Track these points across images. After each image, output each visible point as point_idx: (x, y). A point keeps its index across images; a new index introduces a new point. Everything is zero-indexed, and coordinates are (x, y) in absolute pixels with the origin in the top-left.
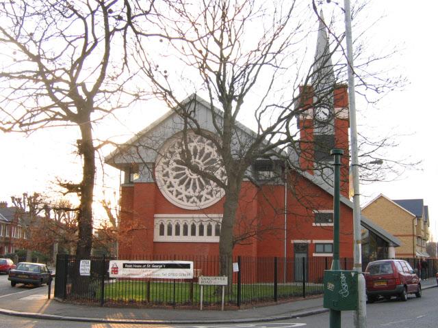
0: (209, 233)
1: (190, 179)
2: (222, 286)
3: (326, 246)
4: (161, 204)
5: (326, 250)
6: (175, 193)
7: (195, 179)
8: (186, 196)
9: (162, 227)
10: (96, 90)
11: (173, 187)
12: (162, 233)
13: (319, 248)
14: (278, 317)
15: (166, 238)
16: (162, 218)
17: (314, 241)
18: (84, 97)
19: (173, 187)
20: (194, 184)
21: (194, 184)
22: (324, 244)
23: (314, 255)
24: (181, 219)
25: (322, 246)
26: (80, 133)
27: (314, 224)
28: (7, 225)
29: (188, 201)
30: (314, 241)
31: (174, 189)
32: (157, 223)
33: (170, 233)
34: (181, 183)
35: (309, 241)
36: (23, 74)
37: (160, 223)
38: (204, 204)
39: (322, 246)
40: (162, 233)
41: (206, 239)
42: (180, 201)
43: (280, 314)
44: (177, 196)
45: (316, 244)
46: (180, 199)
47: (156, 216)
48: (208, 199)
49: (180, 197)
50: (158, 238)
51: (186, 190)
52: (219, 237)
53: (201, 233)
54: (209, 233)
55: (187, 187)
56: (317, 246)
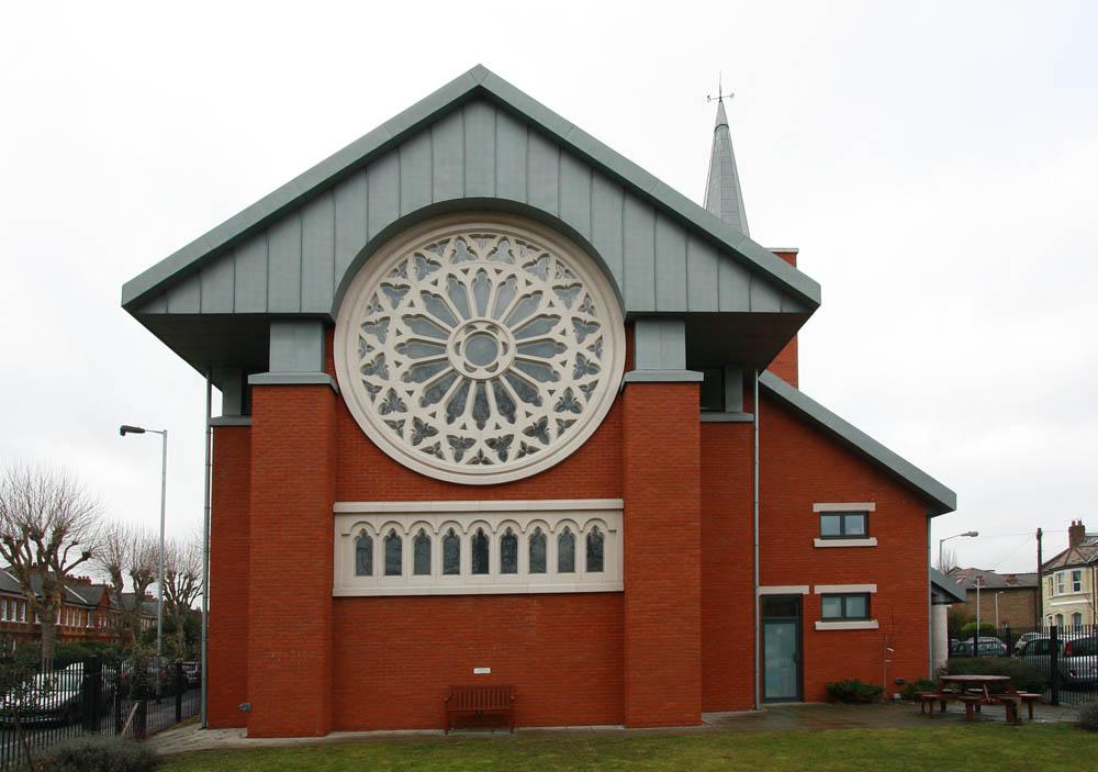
1: (467, 381)
3: (838, 533)
4: (356, 465)
5: (849, 613)
7: (481, 382)
8: (452, 440)
12: (364, 567)
13: (830, 609)
15: (379, 584)
16: (362, 518)
17: (820, 589)
20: (481, 399)
21: (481, 399)
22: (843, 596)
23: (820, 626)
24: (436, 518)
26: (331, 307)
28: (88, 610)
29: (416, 442)
30: (820, 589)
34: (433, 395)
35: (804, 590)
37: (356, 532)
38: (515, 468)
40: (364, 567)
42: (432, 459)
44: (385, 410)
45: (867, 536)
46: (428, 451)
47: (340, 507)
48: (532, 450)
49: (395, 416)
50: (349, 583)
51: (424, 404)
56: (862, 613)
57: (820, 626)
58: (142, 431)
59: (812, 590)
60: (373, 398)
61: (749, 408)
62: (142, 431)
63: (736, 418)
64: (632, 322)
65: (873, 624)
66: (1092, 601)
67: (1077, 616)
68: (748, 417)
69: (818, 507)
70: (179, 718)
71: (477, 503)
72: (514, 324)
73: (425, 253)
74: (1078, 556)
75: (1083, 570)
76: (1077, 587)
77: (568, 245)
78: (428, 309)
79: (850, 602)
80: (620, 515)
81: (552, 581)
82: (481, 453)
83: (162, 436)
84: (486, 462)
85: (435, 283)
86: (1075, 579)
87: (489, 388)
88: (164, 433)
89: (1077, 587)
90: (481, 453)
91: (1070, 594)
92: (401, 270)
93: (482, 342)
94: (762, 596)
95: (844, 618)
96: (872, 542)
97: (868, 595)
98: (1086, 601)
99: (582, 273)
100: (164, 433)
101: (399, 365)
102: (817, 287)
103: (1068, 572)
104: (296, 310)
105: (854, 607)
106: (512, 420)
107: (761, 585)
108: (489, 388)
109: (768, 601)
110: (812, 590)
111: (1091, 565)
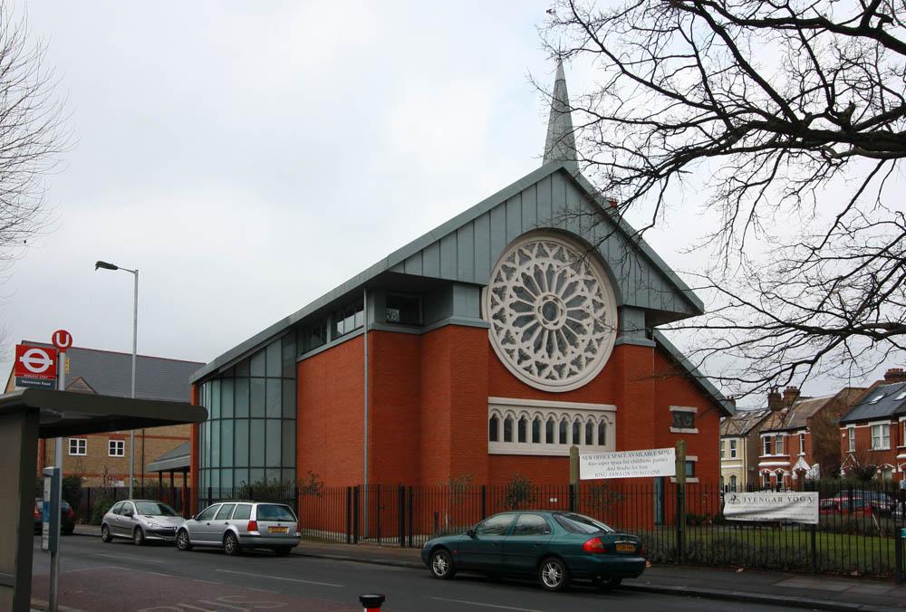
16: (502, 406)
47: (492, 400)
64: (621, 309)
66: (743, 466)
67: (733, 478)
71: (550, 402)
72: (572, 306)
73: (524, 250)
74: (734, 428)
75: (737, 439)
76: (733, 454)
77: (599, 266)
80: (614, 414)
83: (134, 275)
84: (531, 372)
86: (732, 447)
87: (539, 329)
88: (136, 272)
89: (733, 454)
91: (782, 455)
92: (512, 259)
93: (550, 310)
98: (739, 466)
99: (597, 274)
100: (136, 272)
101: (573, 352)
102: (702, 304)
104: (472, 282)
106: (535, 351)
108: (539, 329)
109: (76, 441)
111: (742, 436)
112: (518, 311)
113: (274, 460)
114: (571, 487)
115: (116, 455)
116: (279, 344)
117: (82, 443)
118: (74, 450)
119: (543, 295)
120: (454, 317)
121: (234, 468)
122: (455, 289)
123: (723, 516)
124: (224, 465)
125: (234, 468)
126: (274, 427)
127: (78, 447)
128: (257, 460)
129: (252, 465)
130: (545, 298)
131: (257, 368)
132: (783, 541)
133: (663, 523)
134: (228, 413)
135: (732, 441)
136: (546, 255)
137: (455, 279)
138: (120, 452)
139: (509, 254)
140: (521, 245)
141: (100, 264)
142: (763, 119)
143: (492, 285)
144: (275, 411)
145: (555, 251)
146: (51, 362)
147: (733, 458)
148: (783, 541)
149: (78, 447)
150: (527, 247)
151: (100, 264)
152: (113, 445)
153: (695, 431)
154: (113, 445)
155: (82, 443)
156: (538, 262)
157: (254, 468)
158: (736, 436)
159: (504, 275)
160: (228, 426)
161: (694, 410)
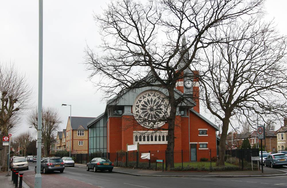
0: (163, 140)
2: (257, 161)
5: (204, 147)
6: (138, 104)
9: (136, 137)
10: (196, 69)
11: (140, 102)
13: (201, 146)
14: (153, 175)
17: (199, 143)
18: (193, 75)
19: (140, 102)
21: (154, 103)
22: (203, 144)
23: (199, 149)
25: (202, 145)
27: (199, 135)
30: (199, 143)
31: (139, 104)
32: (135, 135)
33: (144, 140)
35: (197, 143)
36: (204, 82)
39: (202, 145)
41: (162, 142)
43: (153, 175)
47: (166, 142)
52: (167, 143)
53: (160, 140)
54: (163, 140)
55: (148, 101)
56: (206, 147)
57: (199, 149)
58: (66, 105)
59: (198, 143)
60: (136, 110)
61: (188, 115)
62: (66, 105)
63: (186, 117)
65: (208, 149)
67: (283, 146)
68: (188, 117)
69: (199, 129)
70: (173, 143)
76: (283, 139)
78: (167, 136)
79: (204, 145)
81: (158, 142)
82: (138, 103)
83: (70, 106)
85: (149, 98)
89: (283, 139)
90: (138, 103)
94: (191, 144)
95: (203, 148)
96: (207, 135)
97: (207, 144)
103: (280, 134)
105: (205, 146)
107: (190, 142)
110: (198, 143)
111: (285, 132)
112: (142, 110)
113: (102, 147)
114: (127, 152)
115: (81, 145)
116: (103, 119)
117: (82, 142)
118: (80, 144)
119: (149, 105)
120: (124, 114)
121: (93, 149)
122: (125, 107)
123: (141, 158)
124: (94, 148)
125: (93, 149)
126: (102, 139)
127: (81, 143)
128: (98, 147)
129: (97, 148)
130: (150, 106)
131: (98, 125)
132: (178, 164)
133: (196, 160)
134: (95, 136)
135: (282, 134)
136: (150, 96)
137: (124, 105)
138: (82, 144)
139: (140, 97)
140: (143, 94)
141: (63, 105)
142: (163, 68)
143: (136, 105)
144: (102, 135)
145: (153, 95)
146: (8, 139)
147: (282, 140)
148: (178, 164)
149: (81, 143)
150: (145, 95)
151: (63, 105)
152: (80, 142)
153: (207, 135)
154: (80, 142)
155: (82, 142)
156: (148, 98)
157: (102, 148)
158: (283, 132)
159: (139, 102)
160: (95, 138)
161: (207, 129)
